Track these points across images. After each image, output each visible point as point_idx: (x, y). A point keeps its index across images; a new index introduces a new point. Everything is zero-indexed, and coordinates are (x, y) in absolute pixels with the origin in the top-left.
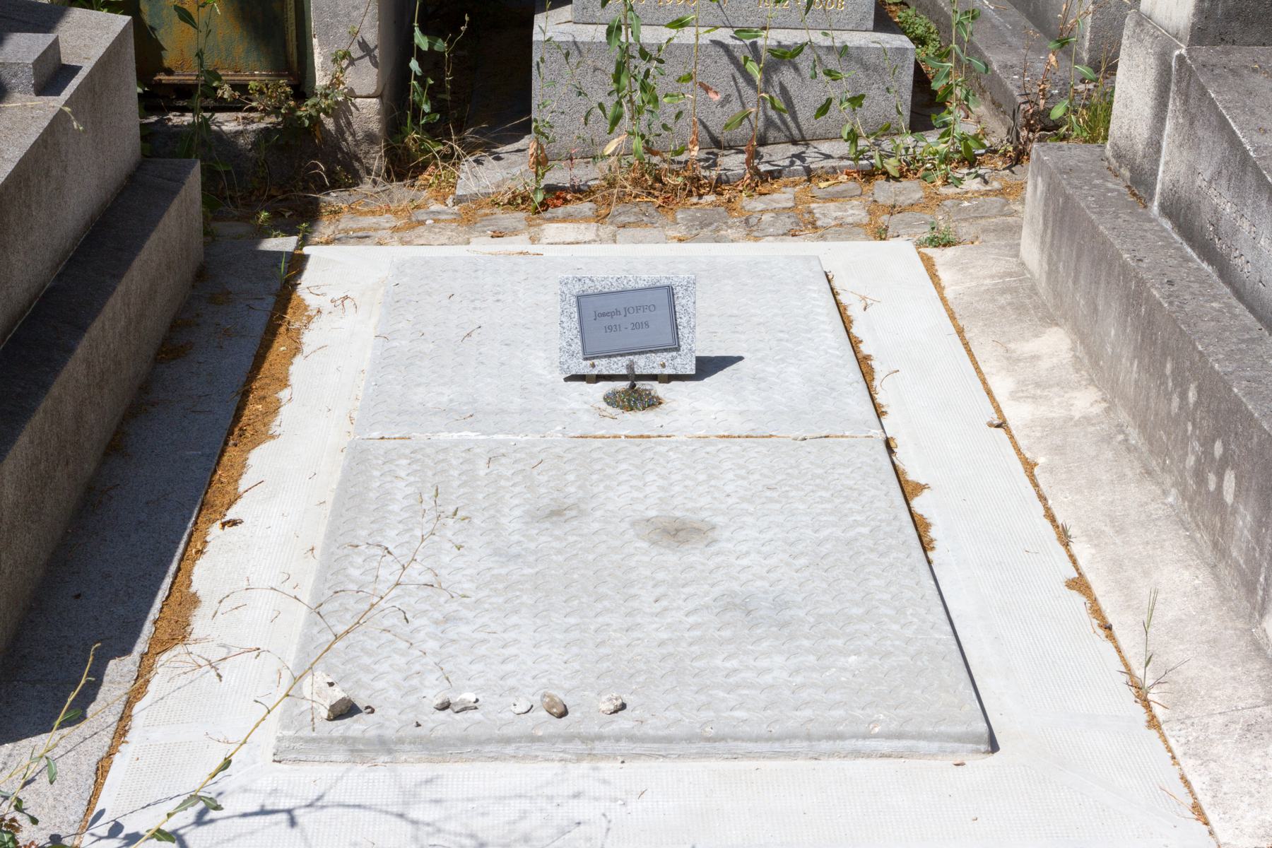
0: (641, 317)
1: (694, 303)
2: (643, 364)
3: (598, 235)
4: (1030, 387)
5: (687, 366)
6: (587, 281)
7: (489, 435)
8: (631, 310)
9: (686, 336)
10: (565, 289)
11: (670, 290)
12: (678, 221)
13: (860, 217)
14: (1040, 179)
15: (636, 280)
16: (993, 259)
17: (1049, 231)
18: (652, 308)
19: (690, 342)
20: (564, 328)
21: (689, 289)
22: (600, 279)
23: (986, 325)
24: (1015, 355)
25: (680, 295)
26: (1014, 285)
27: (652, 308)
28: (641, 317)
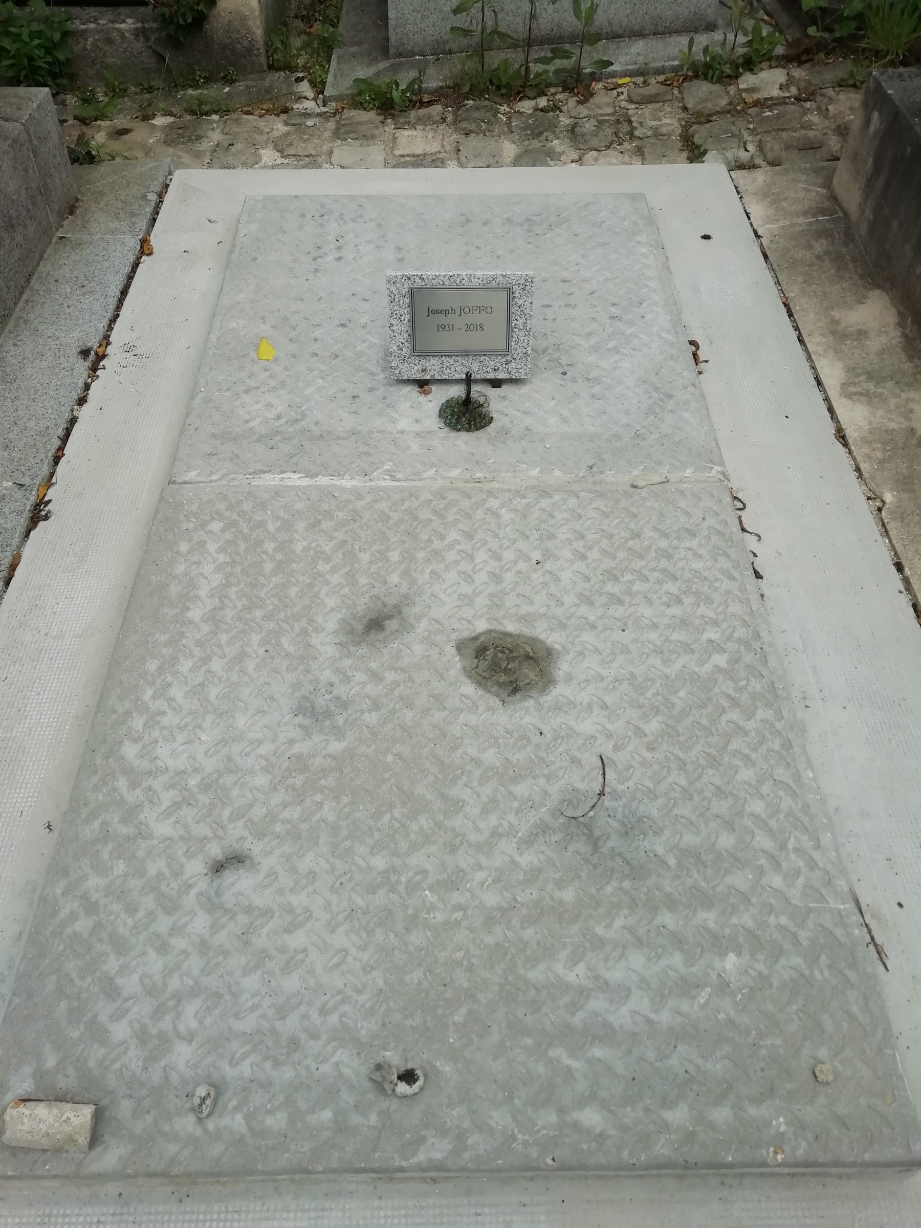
0: (476, 318)
1: (531, 303)
2: (478, 369)
3: (443, 146)
4: (861, 378)
5: (521, 371)
6: (417, 280)
7: (313, 477)
8: (467, 310)
9: (522, 339)
10: (393, 289)
11: (510, 292)
12: (514, 129)
13: (673, 127)
14: (876, 116)
15: (469, 279)
16: (804, 189)
17: (882, 180)
18: (489, 310)
19: (525, 344)
20: (394, 332)
21: (528, 288)
22: (430, 277)
23: (805, 281)
24: (840, 328)
25: (517, 295)
26: (828, 226)
27: (489, 310)
28: (476, 318)
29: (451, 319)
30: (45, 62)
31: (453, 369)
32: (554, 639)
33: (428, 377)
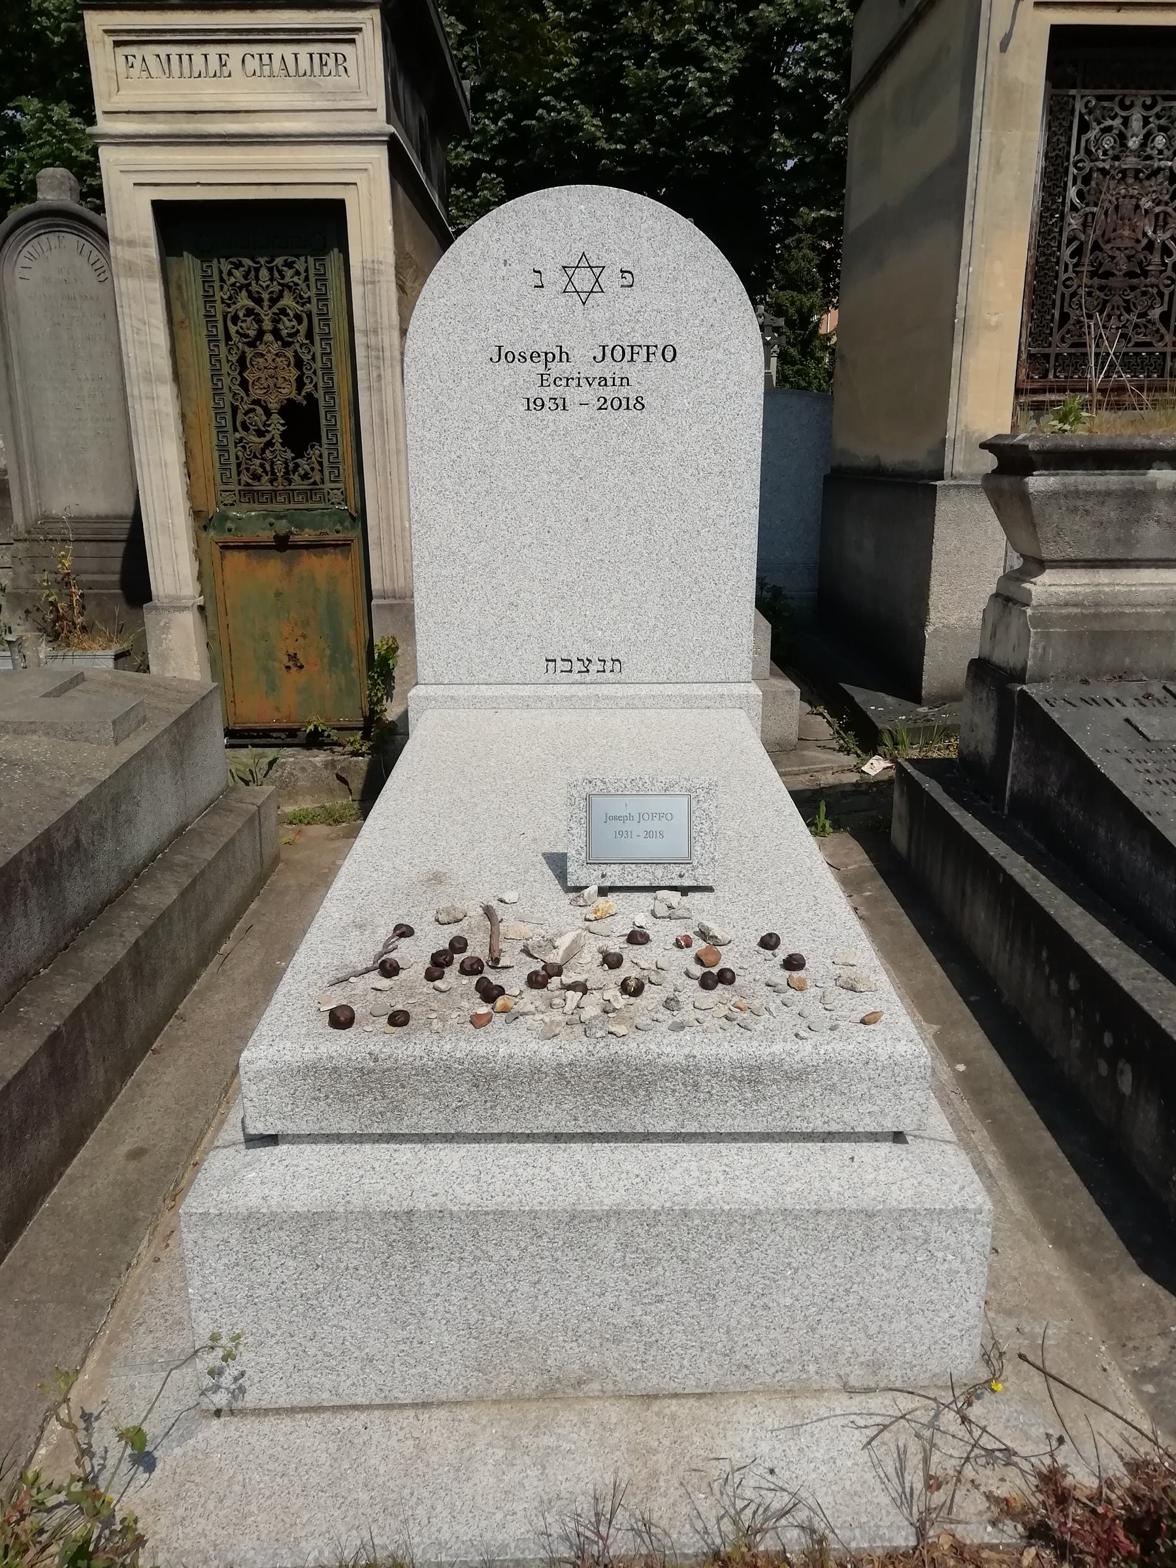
0: (655, 825)
8: (646, 817)
10: (574, 792)
18: (669, 817)
27: (669, 817)
29: (628, 826)
30: (1068, 245)
31: (635, 875)
32: (758, 948)
33: (609, 884)
